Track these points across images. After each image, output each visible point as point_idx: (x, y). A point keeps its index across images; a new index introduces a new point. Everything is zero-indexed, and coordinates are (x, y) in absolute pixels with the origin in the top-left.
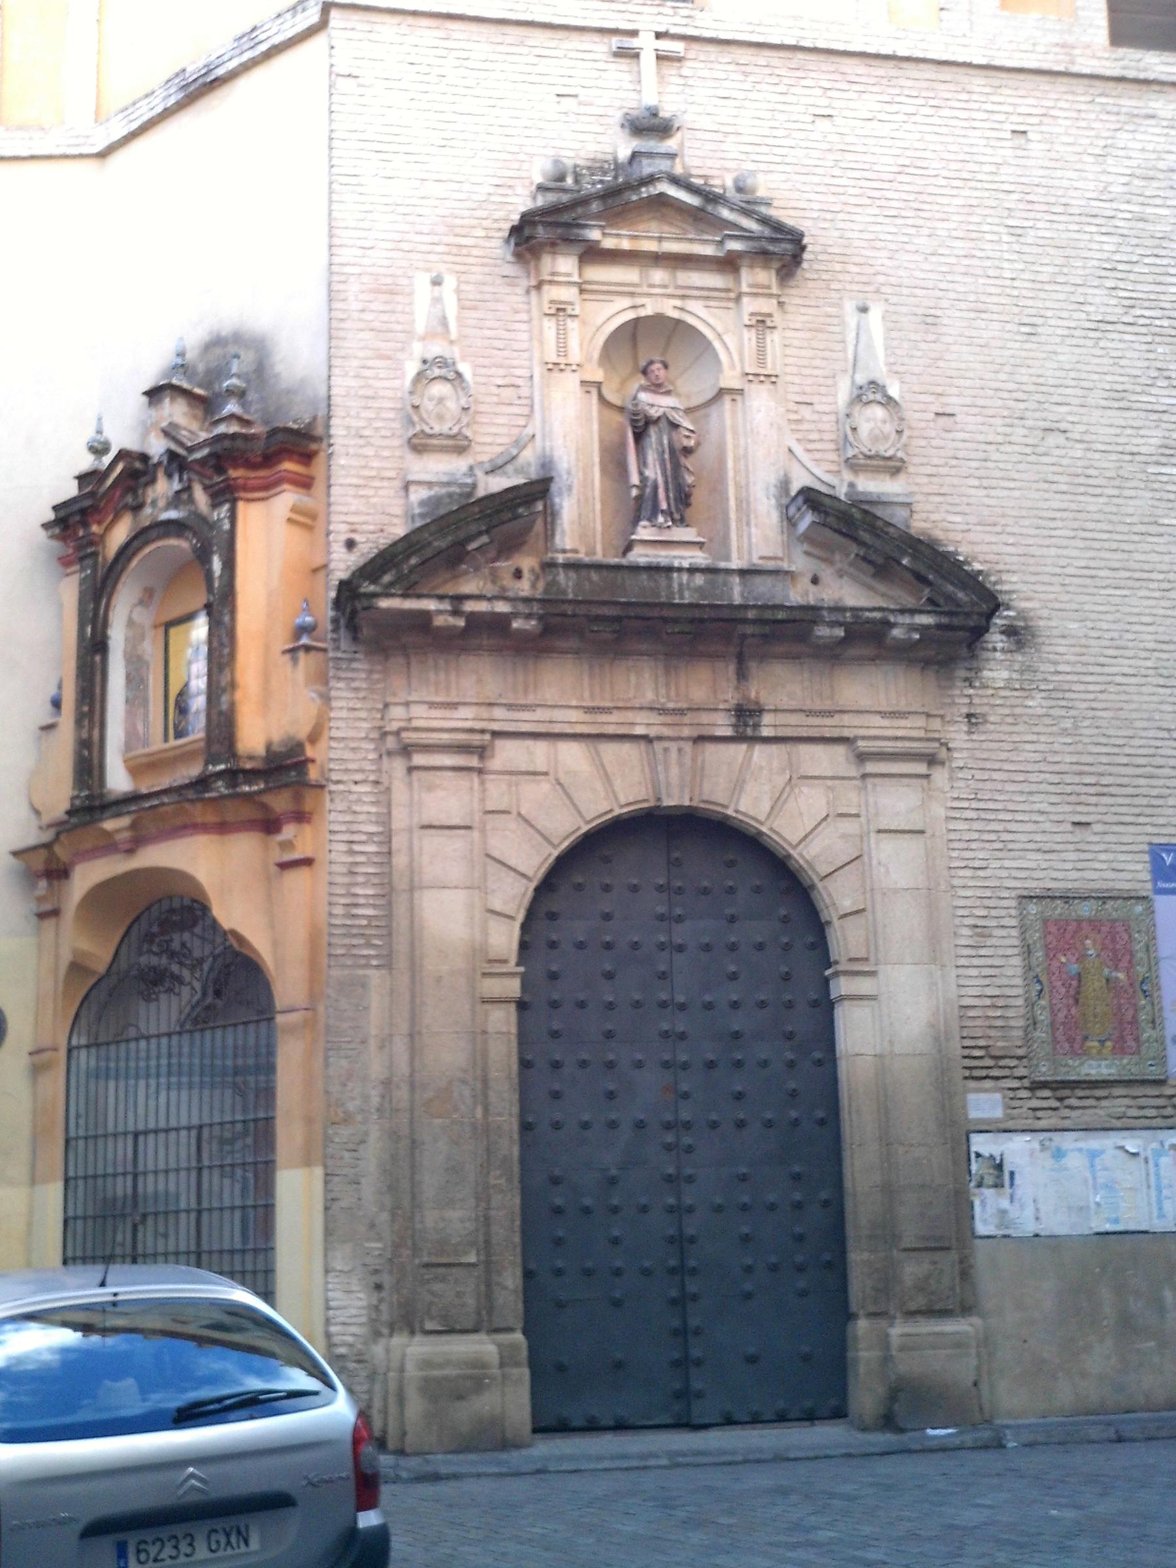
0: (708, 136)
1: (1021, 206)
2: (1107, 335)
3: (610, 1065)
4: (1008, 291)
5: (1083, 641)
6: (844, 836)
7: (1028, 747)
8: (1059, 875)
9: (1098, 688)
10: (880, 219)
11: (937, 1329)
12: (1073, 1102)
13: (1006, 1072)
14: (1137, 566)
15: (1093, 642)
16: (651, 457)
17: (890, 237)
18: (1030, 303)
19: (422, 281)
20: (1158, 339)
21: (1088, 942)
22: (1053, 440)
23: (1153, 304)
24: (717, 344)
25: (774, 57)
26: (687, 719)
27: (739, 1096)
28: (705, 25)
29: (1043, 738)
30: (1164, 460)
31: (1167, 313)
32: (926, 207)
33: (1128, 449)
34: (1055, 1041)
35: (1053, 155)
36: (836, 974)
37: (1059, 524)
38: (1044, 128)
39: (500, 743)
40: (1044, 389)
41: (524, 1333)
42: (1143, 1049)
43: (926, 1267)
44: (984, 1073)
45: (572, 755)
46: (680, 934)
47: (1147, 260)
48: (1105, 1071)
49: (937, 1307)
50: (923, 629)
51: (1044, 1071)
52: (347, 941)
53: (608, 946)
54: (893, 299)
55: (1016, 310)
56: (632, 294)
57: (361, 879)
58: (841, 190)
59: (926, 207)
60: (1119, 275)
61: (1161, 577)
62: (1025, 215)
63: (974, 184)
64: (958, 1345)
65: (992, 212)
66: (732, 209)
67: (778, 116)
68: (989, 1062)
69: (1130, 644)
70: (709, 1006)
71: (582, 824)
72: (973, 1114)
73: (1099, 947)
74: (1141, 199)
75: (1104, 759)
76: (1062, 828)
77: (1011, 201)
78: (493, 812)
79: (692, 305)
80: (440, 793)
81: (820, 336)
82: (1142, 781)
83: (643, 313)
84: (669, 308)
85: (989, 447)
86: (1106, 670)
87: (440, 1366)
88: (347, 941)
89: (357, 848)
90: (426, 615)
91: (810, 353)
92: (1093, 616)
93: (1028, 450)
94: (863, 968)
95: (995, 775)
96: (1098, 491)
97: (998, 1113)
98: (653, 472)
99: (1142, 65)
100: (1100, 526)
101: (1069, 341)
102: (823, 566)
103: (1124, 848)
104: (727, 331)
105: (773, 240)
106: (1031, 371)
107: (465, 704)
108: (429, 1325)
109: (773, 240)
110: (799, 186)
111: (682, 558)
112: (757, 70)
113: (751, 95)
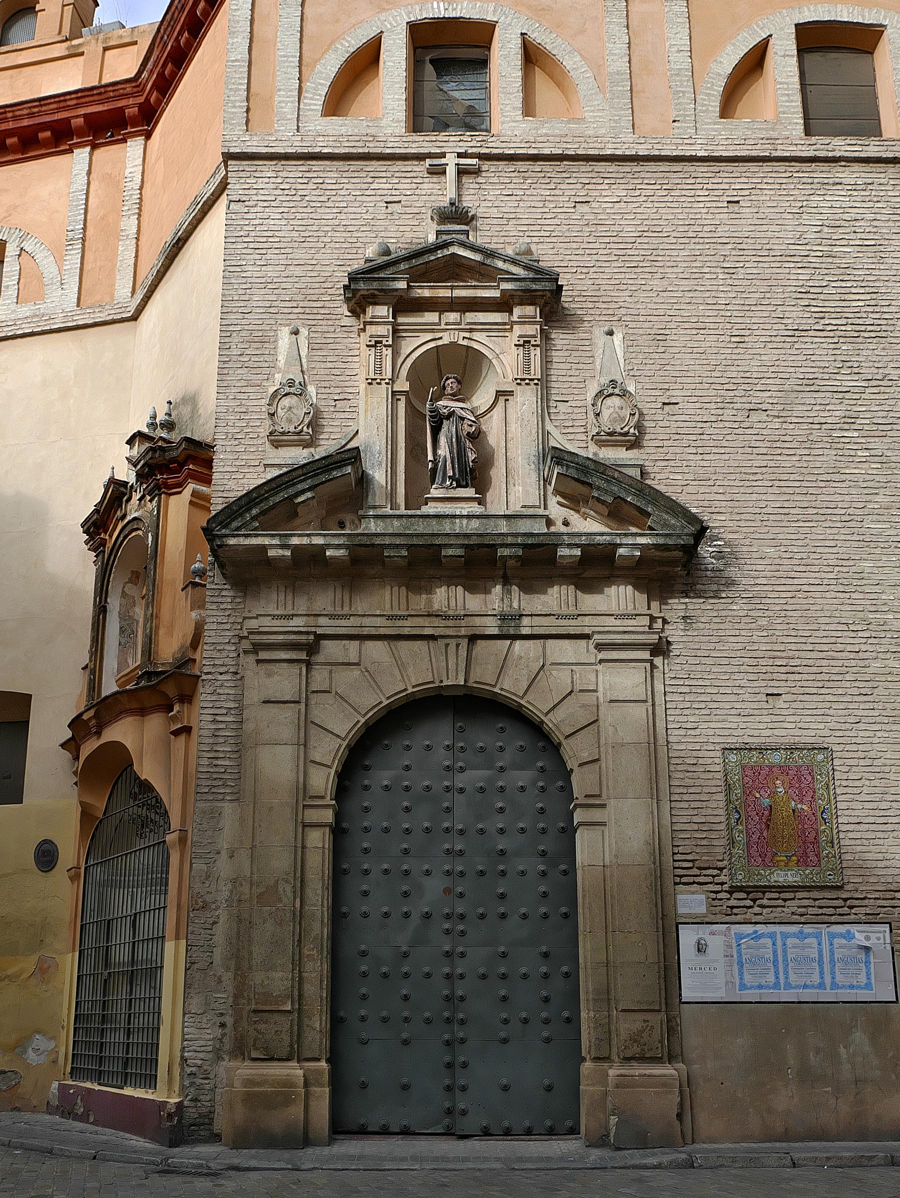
0: (495, 221)
1: (734, 253)
2: (801, 339)
3: (407, 873)
4: (723, 313)
5: (777, 561)
6: (583, 706)
7: (732, 639)
8: (756, 733)
9: (789, 595)
10: (622, 270)
11: (648, 1072)
12: (765, 902)
13: (710, 879)
14: (825, 505)
15: (786, 562)
16: (443, 440)
17: (631, 282)
18: (740, 320)
19: (285, 332)
20: (842, 340)
21: (778, 782)
22: (755, 417)
23: (839, 315)
24: (494, 361)
25: (547, 166)
26: (463, 623)
27: (502, 896)
28: (495, 146)
29: (743, 633)
30: (846, 426)
31: (850, 321)
32: (660, 259)
33: (816, 420)
34: (750, 856)
35: (761, 216)
36: (576, 806)
37: (759, 477)
38: (753, 198)
39: (325, 643)
40: (749, 381)
41: (328, 1061)
42: (823, 862)
43: (639, 1025)
44: (691, 880)
45: (376, 650)
46: (461, 780)
47: (834, 284)
48: (790, 879)
49: (648, 1055)
50: (643, 547)
51: (741, 878)
52: (209, 783)
53: (407, 789)
54: (631, 325)
55: (729, 326)
56: (432, 331)
57: (221, 740)
58: (594, 252)
59: (660, 259)
60: (811, 296)
61: (843, 511)
62: (737, 259)
63: (697, 240)
64: (664, 1085)
65: (711, 258)
66: (505, 261)
67: (547, 204)
68: (695, 871)
69: (816, 562)
70: (482, 831)
71: (383, 699)
72: (681, 910)
73: (787, 785)
74: (829, 242)
75: (793, 647)
76: (759, 697)
77: (726, 250)
78: (317, 692)
79: (476, 336)
80: (276, 678)
81: (575, 354)
82: (825, 663)
83: (440, 343)
84: (460, 338)
85: (704, 425)
86: (796, 581)
87: (259, 1084)
88: (209, 783)
89: (219, 718)
90: (264, 548)
91: (568, 366)
92: (785, 542)
93: (736, 425)
94: (595, 802)
95: (704, 660)
96: (792, 452)
97: (703, 910)
98: (444, 451)
99: (830, 147)
100: (792, 477)
101: (770, 345)
102: (572, 512)
103: (809, 712)
104: (773, 663)
105: (534, 280)
106: (740, 369)
107: (297, 615)
108: (254, 1055)
109: (534, 280)
110: (561, 251)
111: (462, 508)
112: (534, 174)
113: (528, 192)
